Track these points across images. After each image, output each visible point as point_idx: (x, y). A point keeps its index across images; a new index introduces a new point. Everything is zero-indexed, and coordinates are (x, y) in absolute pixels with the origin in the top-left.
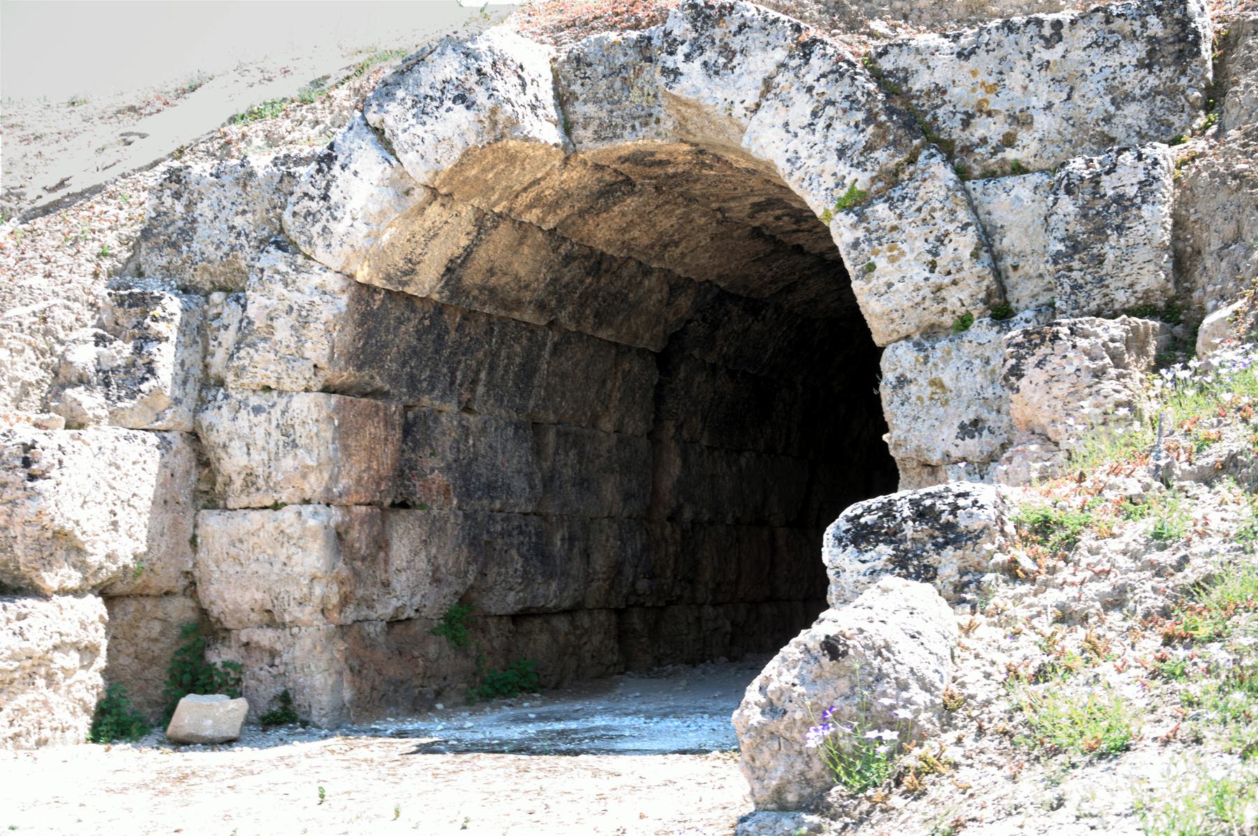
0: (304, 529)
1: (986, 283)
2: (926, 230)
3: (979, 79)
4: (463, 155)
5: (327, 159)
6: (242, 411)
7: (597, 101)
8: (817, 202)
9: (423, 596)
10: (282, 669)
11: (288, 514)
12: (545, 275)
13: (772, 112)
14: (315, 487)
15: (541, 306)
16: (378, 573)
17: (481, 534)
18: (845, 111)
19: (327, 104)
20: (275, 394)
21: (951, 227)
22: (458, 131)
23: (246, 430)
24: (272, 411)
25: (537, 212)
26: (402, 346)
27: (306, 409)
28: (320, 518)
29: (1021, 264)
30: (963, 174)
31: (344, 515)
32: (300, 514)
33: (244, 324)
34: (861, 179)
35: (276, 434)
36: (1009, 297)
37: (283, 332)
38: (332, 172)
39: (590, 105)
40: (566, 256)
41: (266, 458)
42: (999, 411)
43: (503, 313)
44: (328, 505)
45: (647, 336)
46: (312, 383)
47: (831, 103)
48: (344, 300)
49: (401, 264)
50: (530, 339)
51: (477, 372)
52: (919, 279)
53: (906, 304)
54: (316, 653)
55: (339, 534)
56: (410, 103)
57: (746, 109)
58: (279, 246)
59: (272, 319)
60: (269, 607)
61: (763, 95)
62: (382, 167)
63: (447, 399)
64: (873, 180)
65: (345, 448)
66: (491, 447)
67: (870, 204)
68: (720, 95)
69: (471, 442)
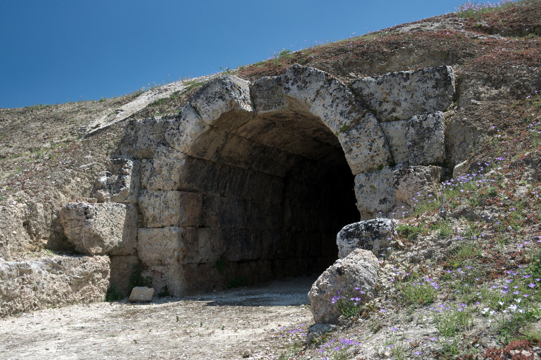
1: (387, 155)
5: (179, 117)
7: (264, 98)
8: (334, 129)
10: (165, 279)
11: (166, 230)
15: (246, 163)
18: (342, 101)
20: (162, 191)
21: (376, 137)
23: (153, 203)
25: (245, 133)
30: (379, 121)
32: (170, 229)
34: (347, 122)
35: (162, 204)
36: (395, 159)
37: (165, 172)
48: (184, 161)
51: (226, 184)
53: (362, 162)
55: (182, 236)
58: (164, 144)
60: (161, 259)
61: (316, 96)
65: (184, 208)
67: (351, 130)
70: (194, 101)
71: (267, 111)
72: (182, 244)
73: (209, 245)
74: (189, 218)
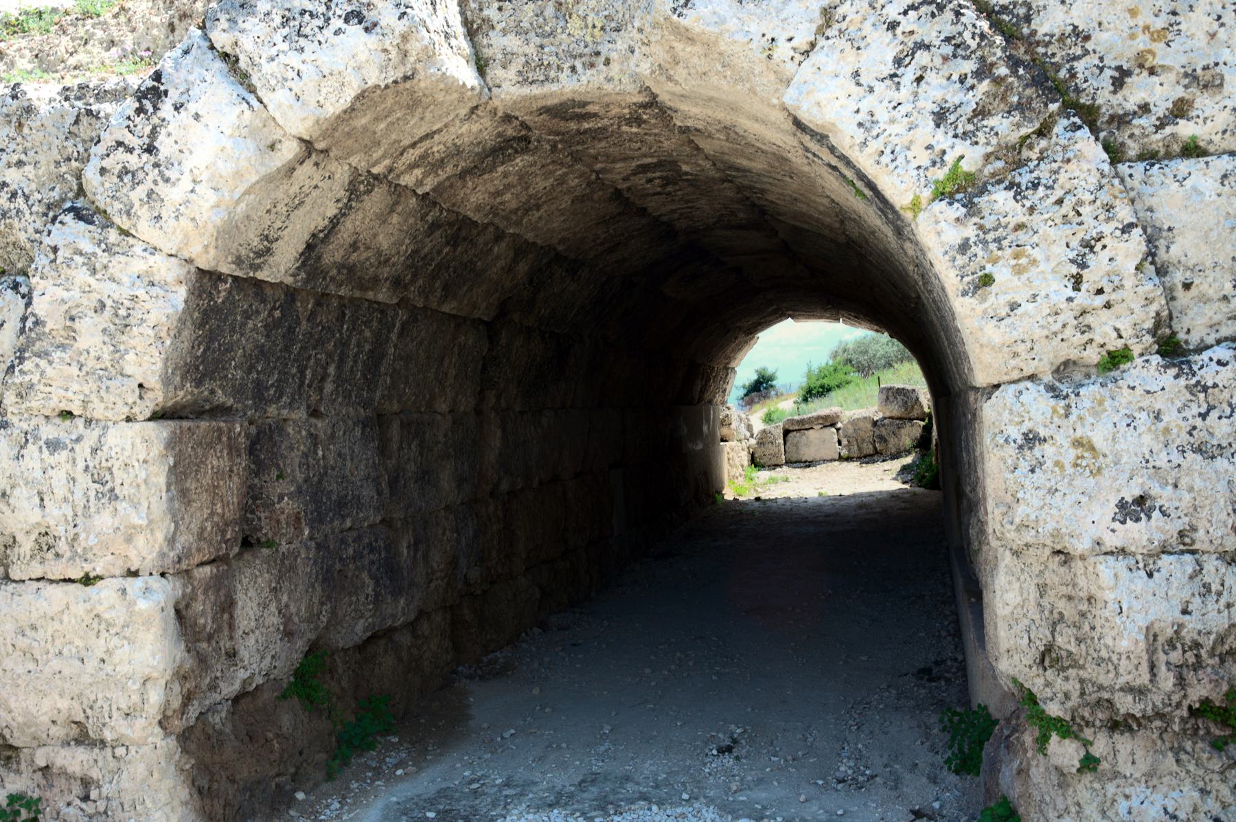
0: (132, 614)
1: (1154, 307)
2: (1068, 230)
3: (1141, 21)
4: (357, 98)
5: (153, 94)
6: (30, 445)
7: (520, 31)
8: (899, 188)
9: (273, 657)
10: (101, 806)
11: (105, 592)
12: (407, 247)
13: (837, 55)
14: (144, 554)
15: (397, 283)
16: (222, 644)
17: (333, 565)
18: (945, 59)
19: (122, 19)
20: (80, 422)
21: (1107, 229)
22: (352, 63)
23: (38, 474)
24: (77, 447)
25: (418, 172)
26: (249, 346)
27: (129, 447)
28: (155, 597)
29: (1196, 282)
30: (1115, 154)
31: (184, 586)
32: (124, 591)
33: (29, 324)
34: (971, 157)
35: (84, 481)
36: (1176, 326)
37: (90, 334)
38: (160, 114)
39: (511, 37)
40: (433, 223)
41: (70, 513)
42: (1176, 486)
43: (357, 294)
44: (163, 575)
45: (484, 304)
46: (136, 410)
47: (924, 46)
48: (182, 293)
49: (255, 242)
50: (380, 321)
51: (325, 368)
52: (1059, 299)
53: (1038, 333)
54: (152, 781)
55: (178, 612)
56: (278, 20)
57: (794, 49)
58: (79, 215)
59: (72, 319)
60: (80, 717)
61: (820, 31)
62: (238, 110)
63: (296, 405)
64: (987, 157)
65: (184, 493)
66: (340, 455)
67: (983, 191)
68: (754, 28)
69: (320, 453)
70: (223, 23)
71: (536, 90)
72: (180, 652)
73: (273, 619)
74: (203, 529)
